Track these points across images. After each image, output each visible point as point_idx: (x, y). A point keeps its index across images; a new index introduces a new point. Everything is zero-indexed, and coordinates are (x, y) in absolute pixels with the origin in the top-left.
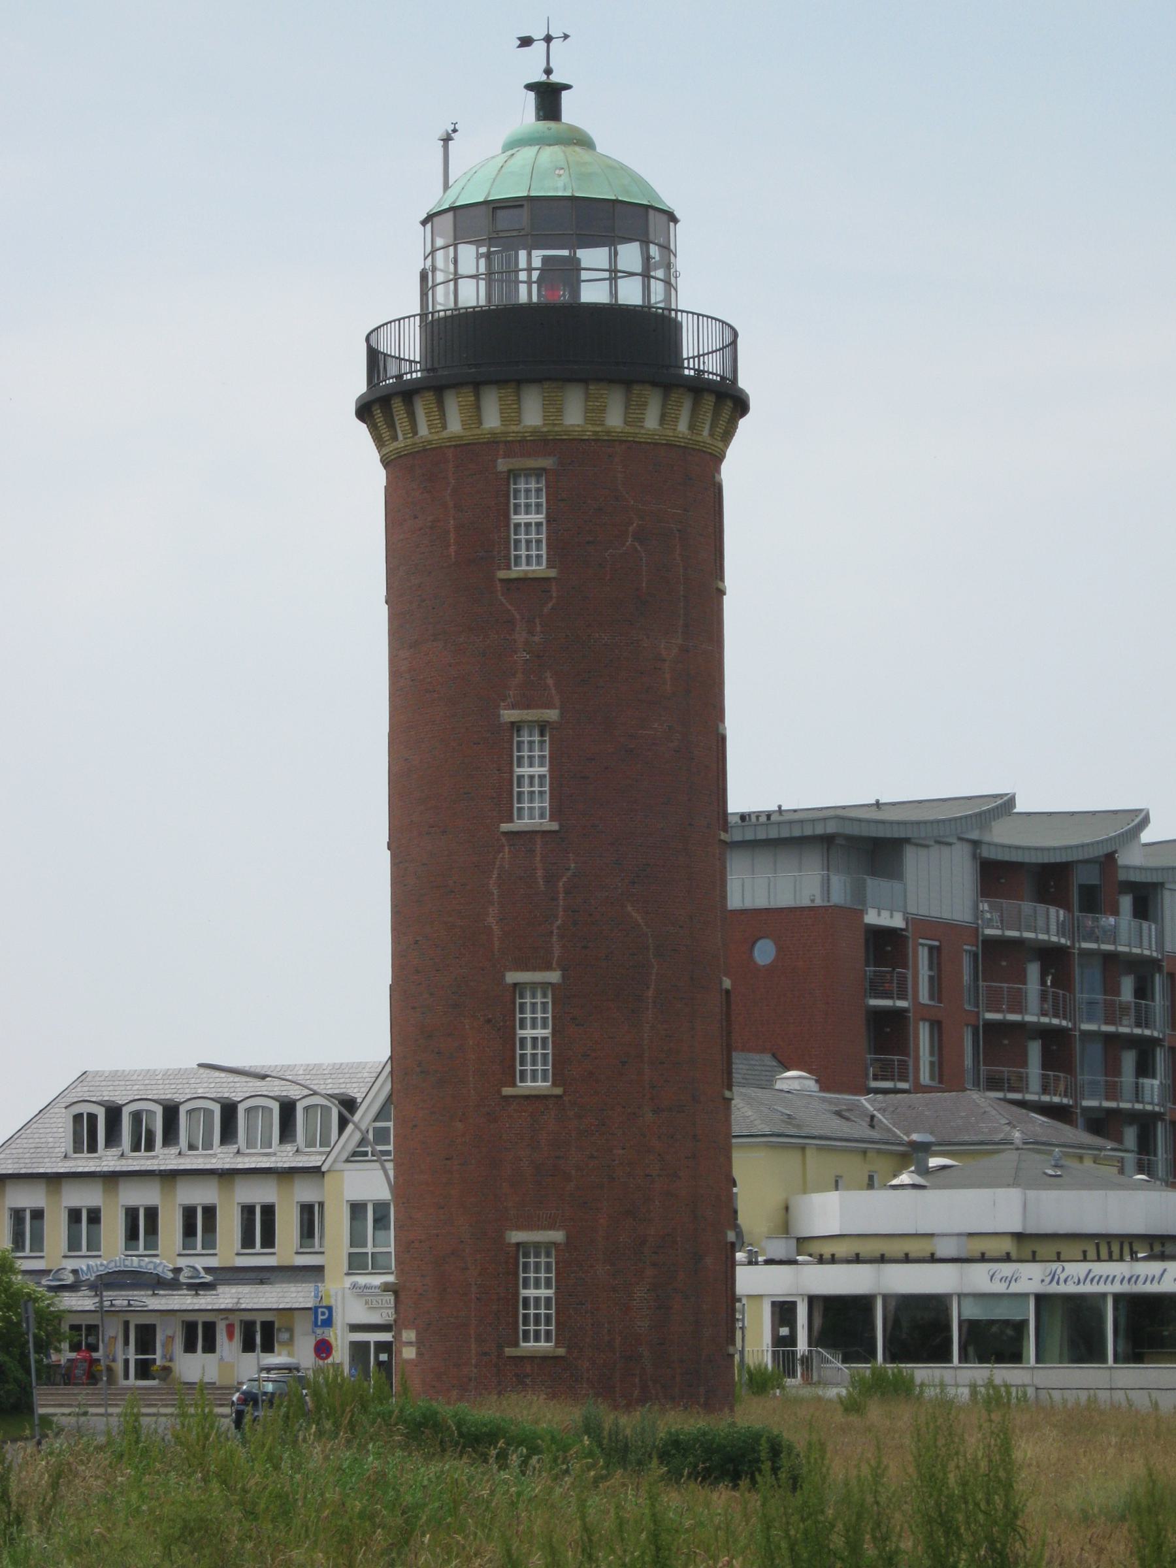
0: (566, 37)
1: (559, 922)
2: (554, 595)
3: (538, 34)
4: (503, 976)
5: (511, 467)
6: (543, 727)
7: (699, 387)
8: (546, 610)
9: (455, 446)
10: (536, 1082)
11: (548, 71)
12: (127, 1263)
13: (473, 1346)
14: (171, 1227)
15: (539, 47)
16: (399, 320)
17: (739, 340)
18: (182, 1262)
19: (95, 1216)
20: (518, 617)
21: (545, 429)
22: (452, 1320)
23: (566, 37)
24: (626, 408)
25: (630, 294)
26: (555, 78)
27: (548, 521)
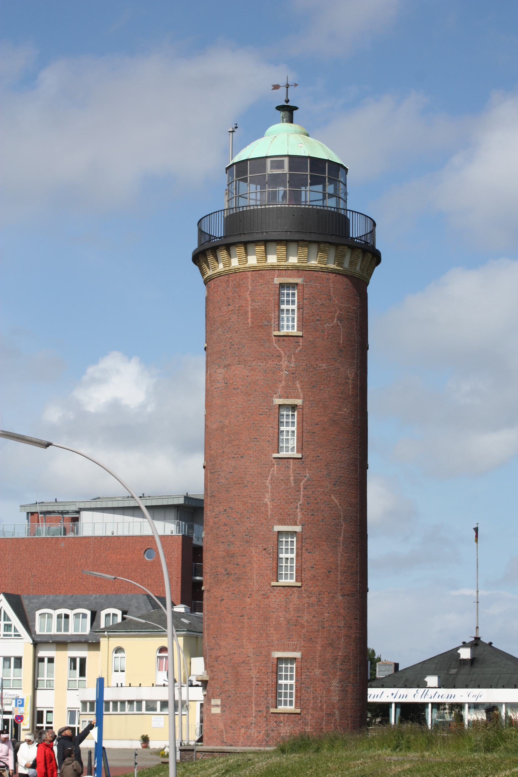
1: (301, 502)
2: (301, 344)
4: (273, 527)
5: (281, 282)
6: (294, 407)
10: (288, 580)
13: (254, 707)
17: (377, 229)
21: (298, 265)
22: (242, 695)
23: (296, 85)
25: (331, 203)
27: (298, 309)
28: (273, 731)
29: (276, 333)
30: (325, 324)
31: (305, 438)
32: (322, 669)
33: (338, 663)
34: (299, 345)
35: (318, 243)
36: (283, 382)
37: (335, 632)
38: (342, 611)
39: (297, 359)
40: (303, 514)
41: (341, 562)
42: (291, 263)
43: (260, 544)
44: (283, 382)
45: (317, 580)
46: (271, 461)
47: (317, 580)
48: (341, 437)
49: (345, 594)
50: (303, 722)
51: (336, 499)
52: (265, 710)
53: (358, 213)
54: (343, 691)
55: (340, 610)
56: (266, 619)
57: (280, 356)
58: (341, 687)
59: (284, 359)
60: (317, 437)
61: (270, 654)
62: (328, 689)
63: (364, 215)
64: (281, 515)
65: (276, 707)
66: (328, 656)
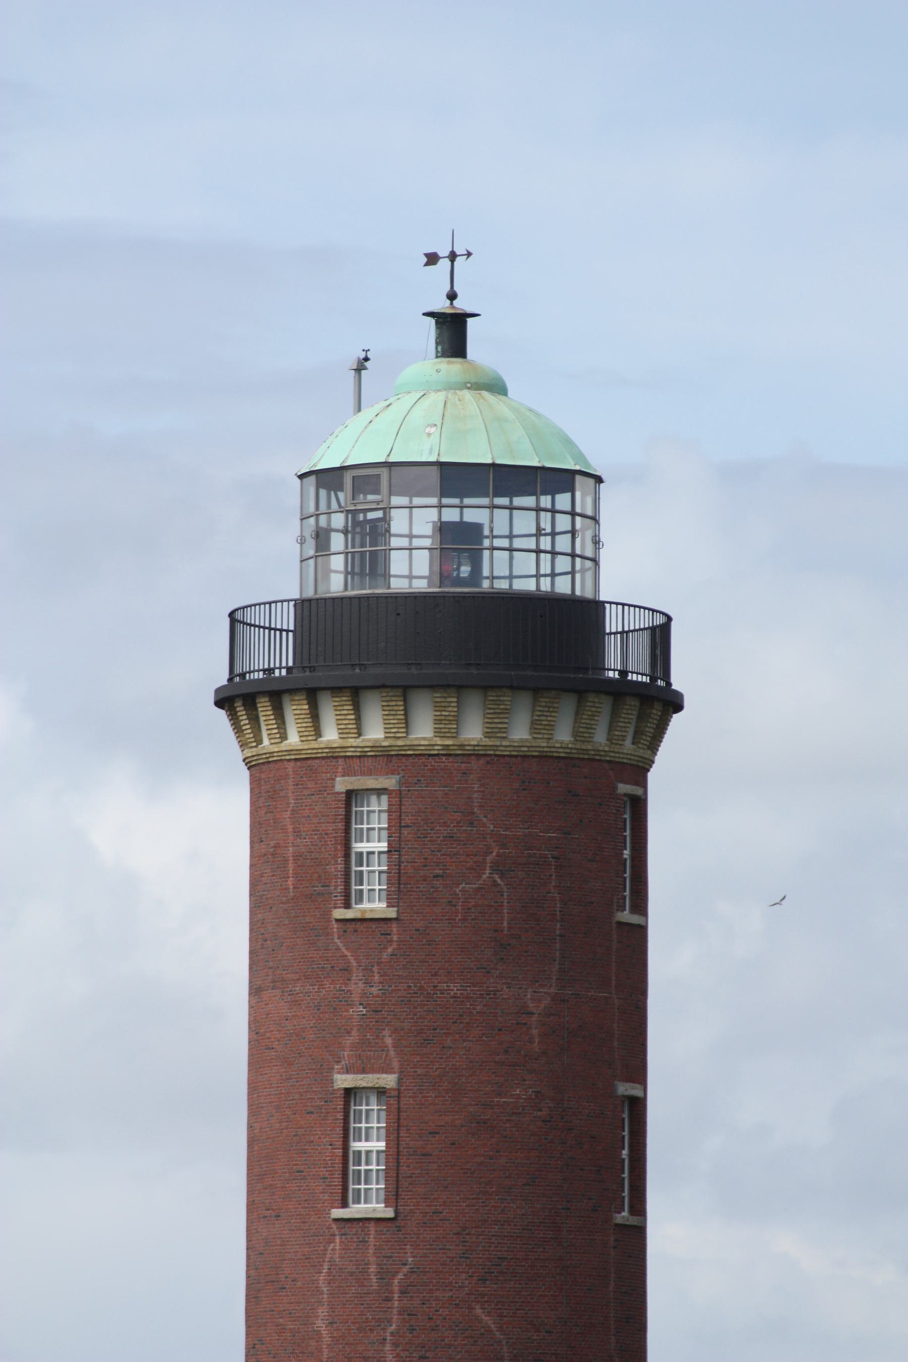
0: (469, 254)
1: (394, 1327)
2: (395, 938)
3: (444, 252)
5: (350, 787)
6: (381, 1092)
7: (621, 690)
8: (385, 955)
9: (296, 760)
11: (452, 296)
15: (444, 264)
16: (270, 603)
21: (386, 744)
23: (469, 254)
24: (575, 722)
26: (461, 305)
29: (340, 913)
31: (403, 1169)
34: (391, 941)
35: (485, 688)
36: (355, 1033)
39: (385, 974)
40: (398, 1355)
42: (369, 740)
44: (355, 1033)
46: (329, 1228)
51: (489, 1314)
53: (635, 606)
57: (347, 970)
59: (357, 975)
60: (435, 1166)
63: (649, 609)
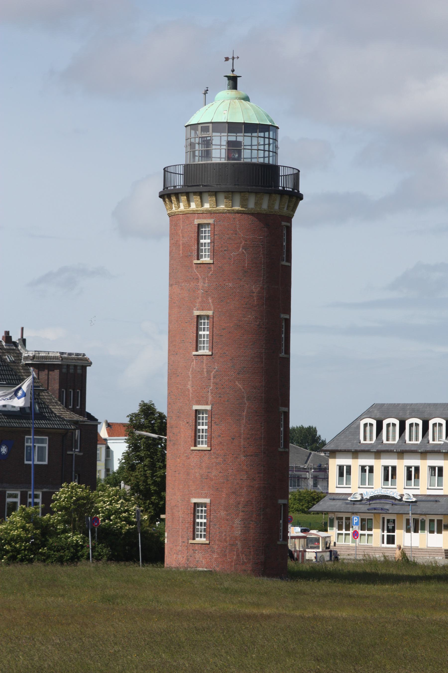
0: (238, 58)
3: (230, 57)
11: (233, 71)
12: (382, 491)
14: (401, 474)
15: (231, 61)
18: (405, 492)
19: (371, 469)
20: (200, 277)
23: (238, 58)
26: (236, 73)
28: (191, 556)
30: (232, 253)
32: (226, 511)
33: (240, 506)
34: (211, 270)
36: (200, 298)
37: (238, 484)
38: (245, 467)
39: (209, 280)
41: (244, 431)
43: (185, 419)
44: (200, 298)
45: (223, 445)
46: (192, 358)
47: (223, 445)
48: (245, 337)
49: (248, 454)
50: (211, 550)
51: (240, 384)
52: (186, 542)
54: (245, 527)
55: (243, 467)
56: (188, 474)
57: (198, 279)
58: (243, 524)
59: (201, 281)
60: (224, 339)
61: (189, 500)
62: (231, 526)
64: (198, 397)
65: (326, 531)
66: (231, 501)
